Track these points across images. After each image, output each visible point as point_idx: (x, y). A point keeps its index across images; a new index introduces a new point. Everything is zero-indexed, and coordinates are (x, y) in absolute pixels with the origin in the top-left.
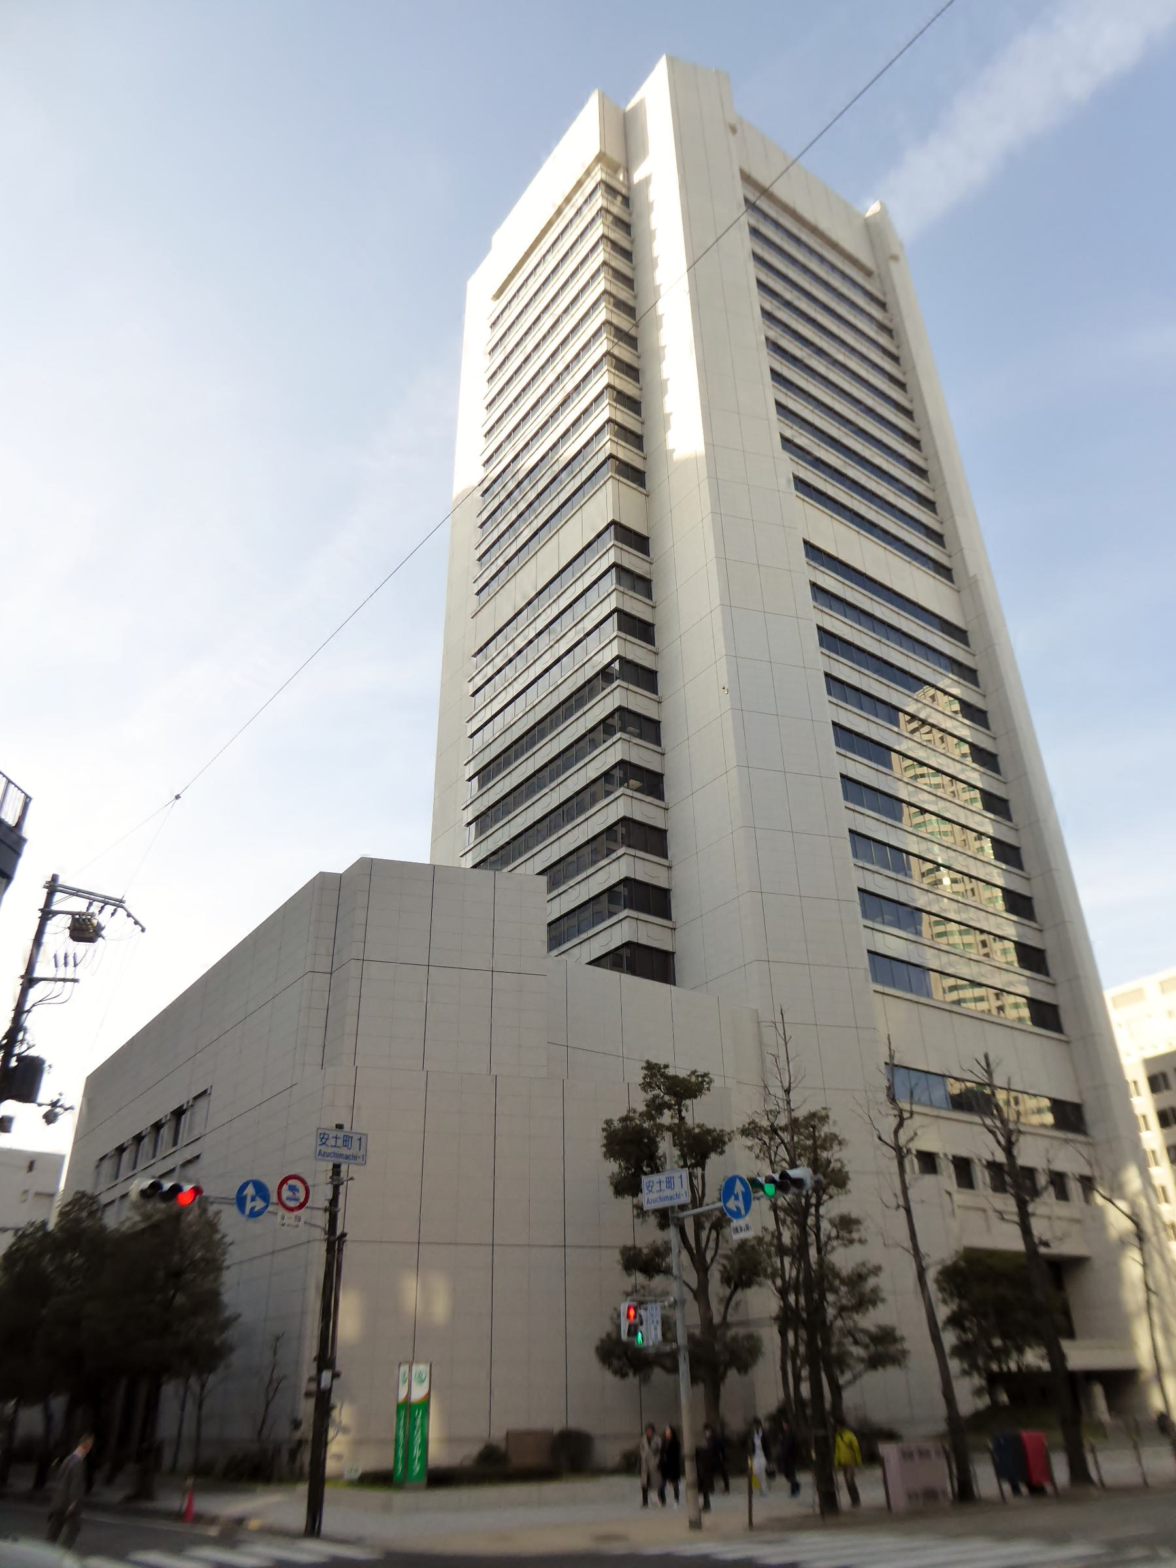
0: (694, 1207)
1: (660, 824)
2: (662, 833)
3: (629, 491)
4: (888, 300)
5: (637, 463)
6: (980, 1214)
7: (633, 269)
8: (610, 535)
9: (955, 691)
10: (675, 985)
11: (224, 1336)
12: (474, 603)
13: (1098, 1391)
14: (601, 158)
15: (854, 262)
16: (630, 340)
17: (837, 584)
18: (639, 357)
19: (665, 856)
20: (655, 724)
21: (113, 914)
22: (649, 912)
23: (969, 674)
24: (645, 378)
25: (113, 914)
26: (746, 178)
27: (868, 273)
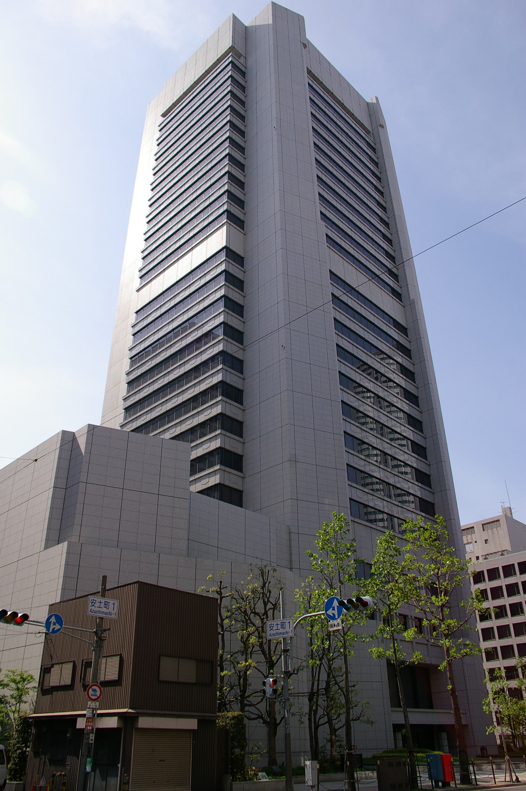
0: (498, 616)
1: (240, 419)
2: (241, 423)
3: (236, 231)
4: (377, 147)
5: (240, 276)
6: (411, 643)
7: (246, 82)
8: (223, 254)
9: (399, 360)
10: (241, 505)
11: (469, 572)
12: (137, 282)
13: (444, 735)
14: (232, 49)
15: (362, 125)
16: (241, 203)
17: (344, 297)
18: (245, 126)
19: (241, 436)
20: (241, 307)
21: (105, 578)
22: (230, 467)
23: (406, 351)
24: (248, 76)
25: (105, 578)
26: (309, 72)
27: (368, 132)
